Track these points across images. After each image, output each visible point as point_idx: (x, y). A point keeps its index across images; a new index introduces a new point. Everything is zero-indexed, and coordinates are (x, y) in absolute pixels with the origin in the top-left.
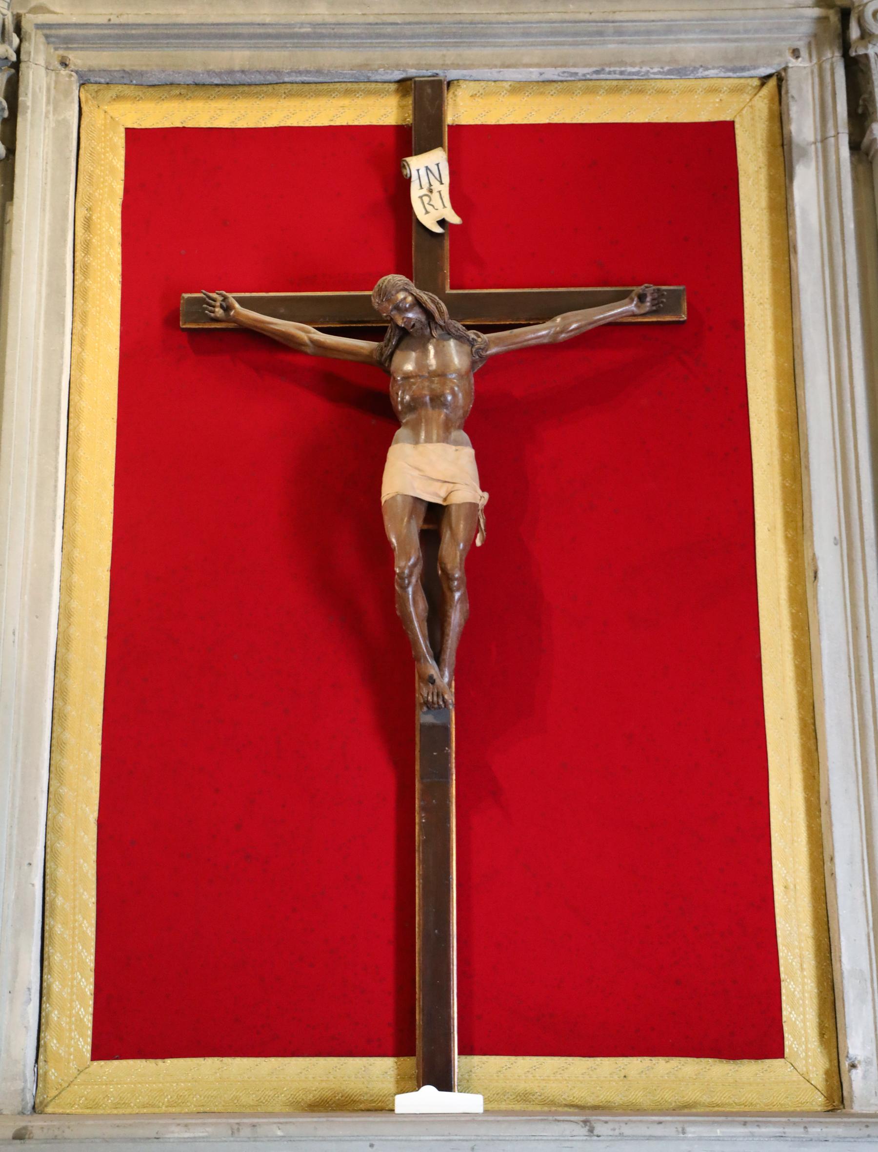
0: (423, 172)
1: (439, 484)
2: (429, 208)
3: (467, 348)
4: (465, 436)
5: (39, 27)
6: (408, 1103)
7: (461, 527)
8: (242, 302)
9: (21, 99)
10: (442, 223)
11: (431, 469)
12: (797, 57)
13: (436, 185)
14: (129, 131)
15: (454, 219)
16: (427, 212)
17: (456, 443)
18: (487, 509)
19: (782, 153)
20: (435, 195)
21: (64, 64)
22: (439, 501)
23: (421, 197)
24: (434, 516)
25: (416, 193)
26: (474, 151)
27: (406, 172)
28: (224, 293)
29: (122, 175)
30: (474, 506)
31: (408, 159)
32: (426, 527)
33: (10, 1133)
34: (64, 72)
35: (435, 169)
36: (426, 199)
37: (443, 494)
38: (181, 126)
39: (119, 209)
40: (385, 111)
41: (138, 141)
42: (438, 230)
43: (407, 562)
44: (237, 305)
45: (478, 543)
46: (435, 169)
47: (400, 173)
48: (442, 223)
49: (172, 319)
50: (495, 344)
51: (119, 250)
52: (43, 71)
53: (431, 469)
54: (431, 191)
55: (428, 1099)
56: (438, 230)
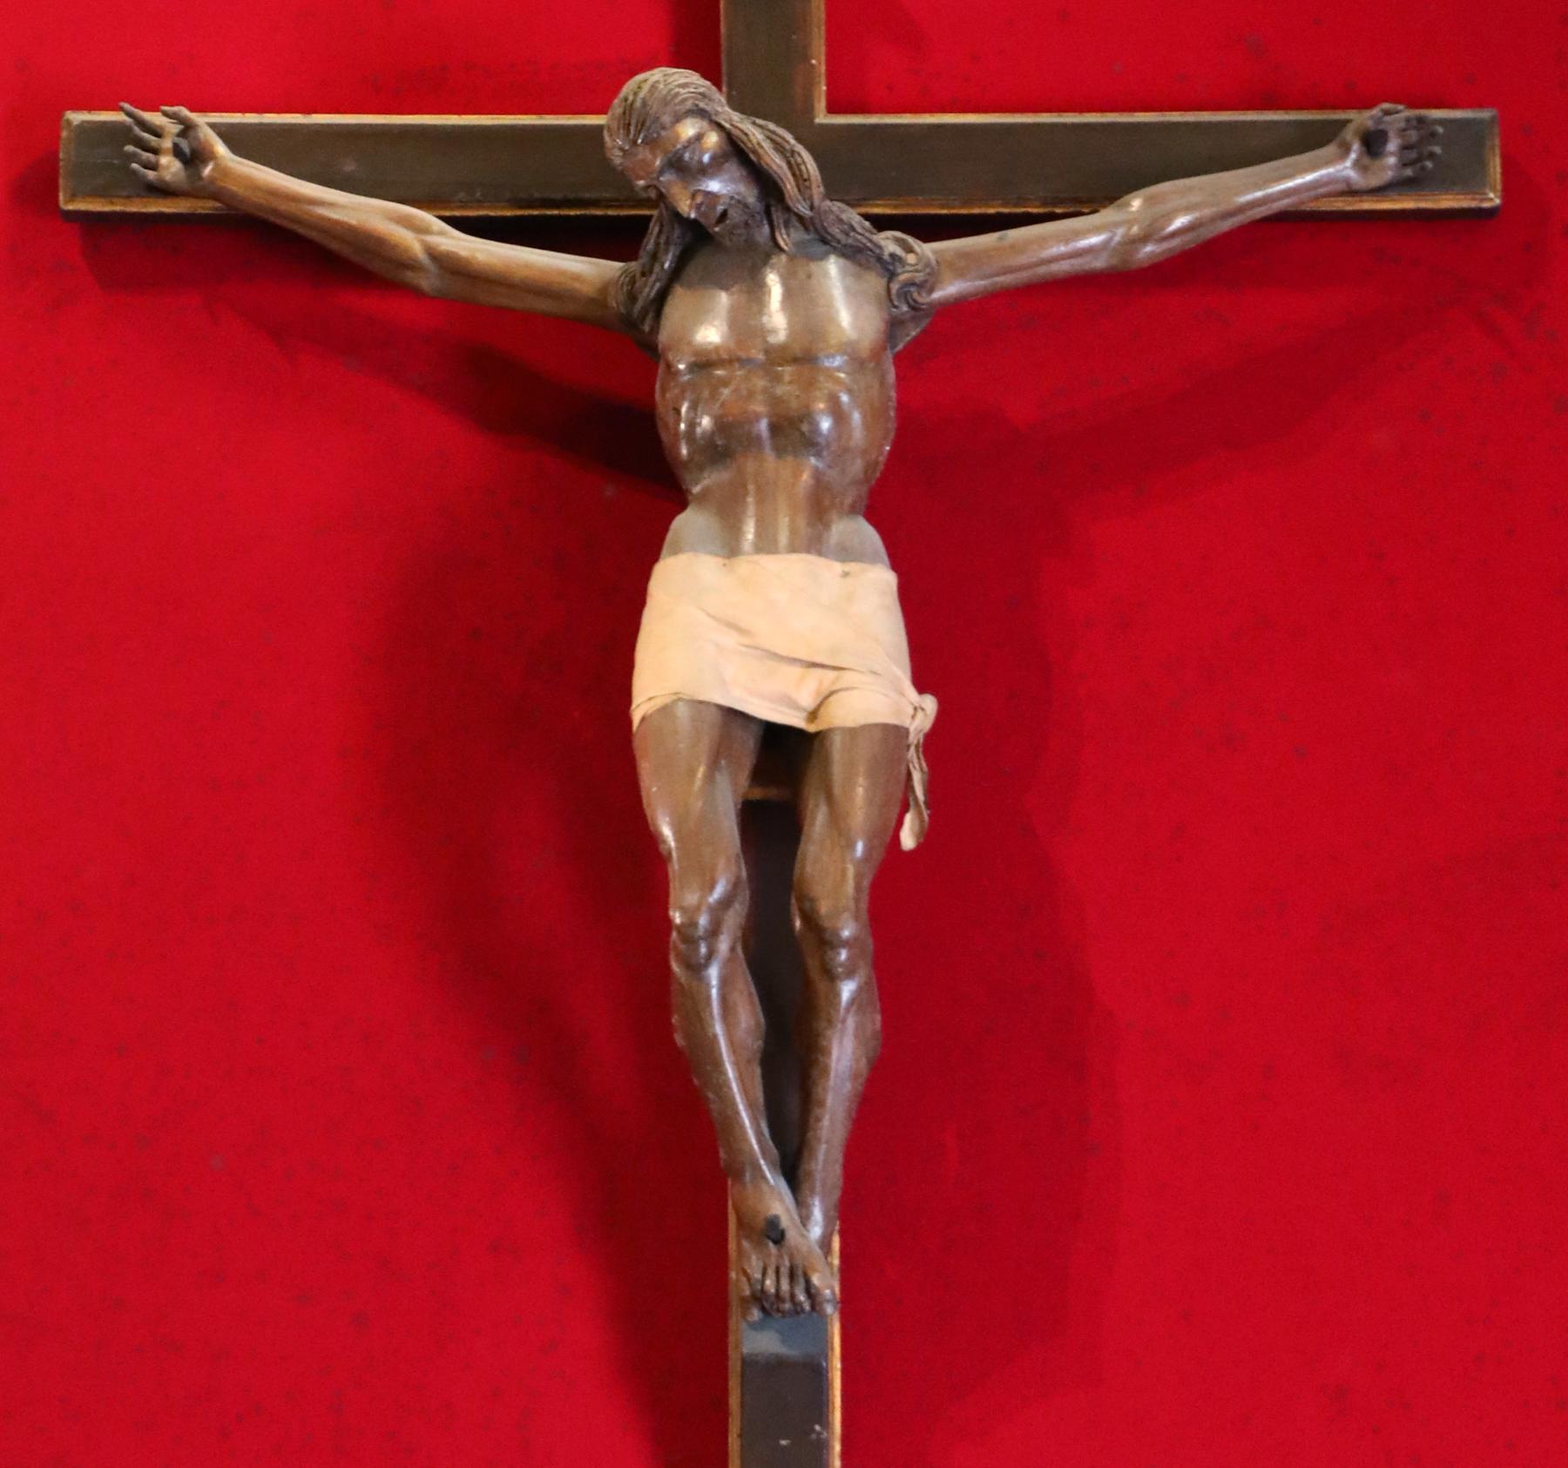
1: (797, 671)
7: (858, 796)
8: (237, 139)
11: (771, 625)
17: (845, 554)
18: (934, 743)
22: (796, 720)
24: (782, 759)
28: (184, 111)
30: (895, 734)
32: (757, 794)
37: (807, 700)
44: (221, 149)
45: (908, 840)
49: (39, 185)
53: (771, 625)
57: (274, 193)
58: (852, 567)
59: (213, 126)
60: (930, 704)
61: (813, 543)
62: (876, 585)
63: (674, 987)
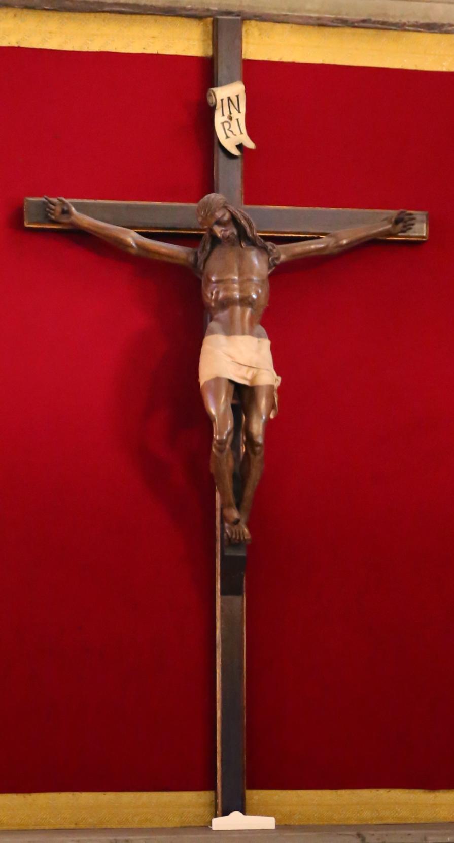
0: (226, 102)
1: (246, 368)
2: (229, 133)
3: (265, 257)
6: (220, 823)
7: (263, 403)
8: (79, 207)
10: (240, 147)
11: (237, 357)
15: (250, 145)
16: (227, 137)
17: (259, 336)
18: (281, 390)
22: (246, 383)
23: (223, 124)
24: (242, 396)
26: (269, 84)
27: (211, 100)
28: (63, 199)
30: (272, 387)
31: (214, 89)
32: (235, 402)
35: (235, 100)
36: (227, 126)
37: (249, 376)
38: (16, 45)
40: (185, 41)
42: (236, 152)
44: (73, 209)
45: (272, 416)
46: (235, 100)
48: (240, 147)
49: (18, 215)
50: (283, 253)
53: (237, 357)
54: (231, 118)
55: (235, 821)
57: (97, 227)
58: (260, 340)
59: (72, 203)
60: (279, 378)
61: (251, 333)
62: (267, 343)
63: (212, 457)
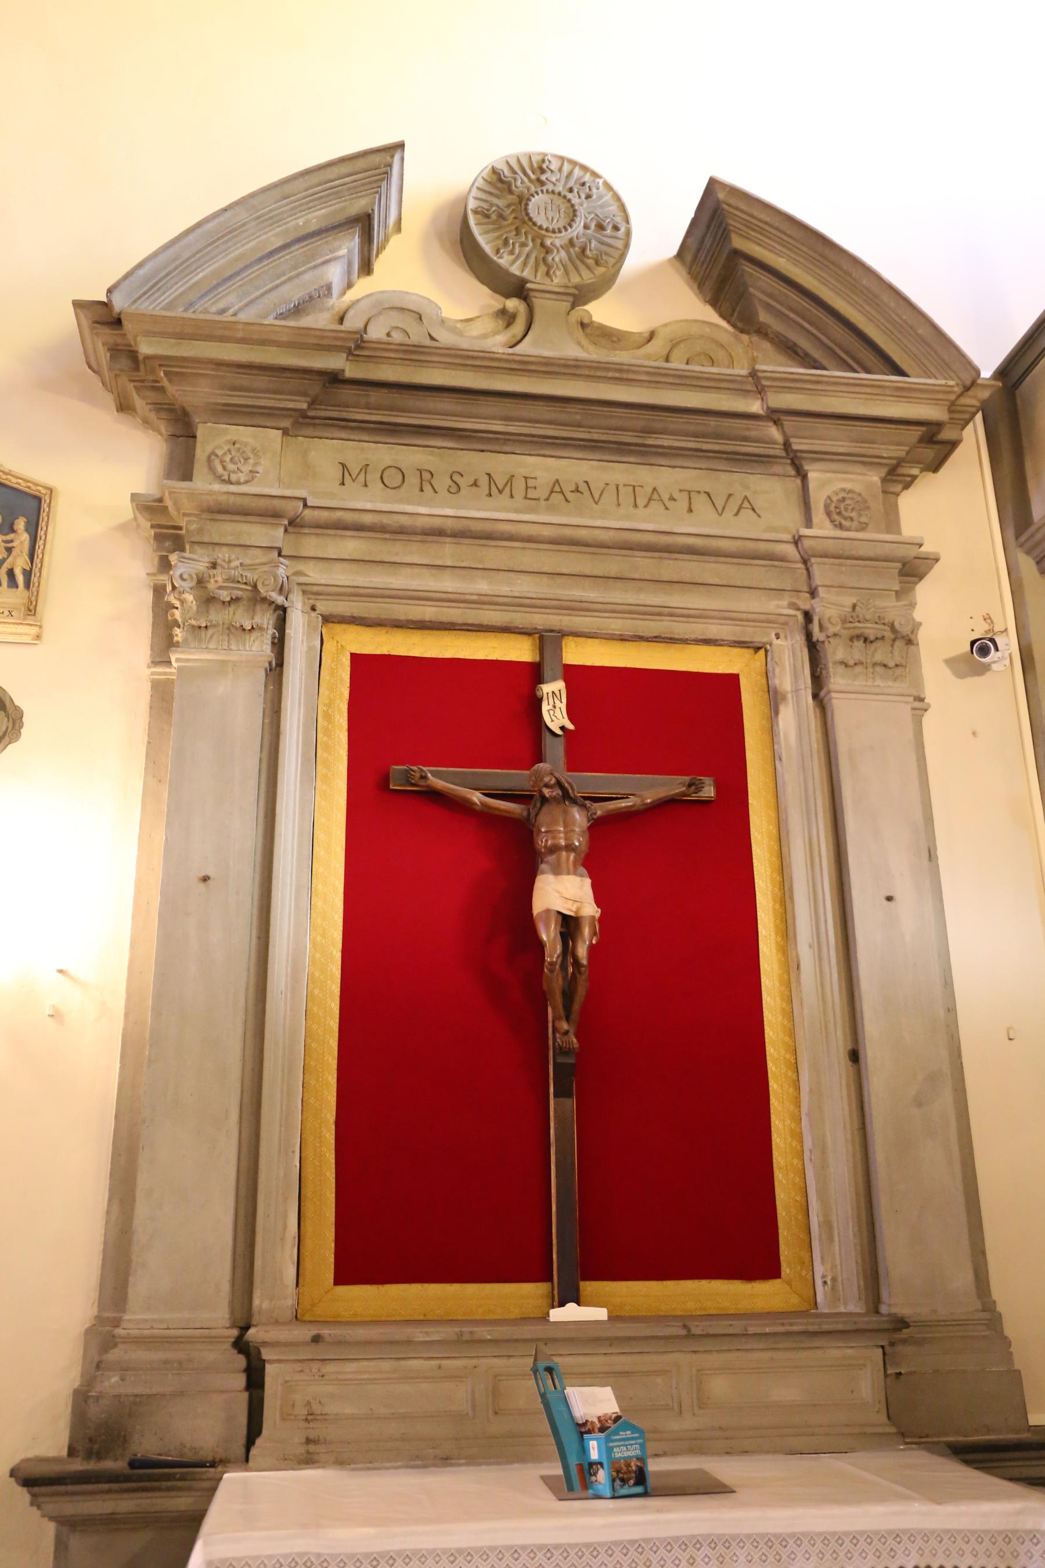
0: (550, 695)
3: (585, 813)
4: (585, 871)
5: (298, 584)
7: (586, 931)
9: (287, 631)
10: (562, 728)
11: (563, 892)
12: (778, 638)
13: (557, 702)
14: (354, 656)
15: (570, 726)
17: (581, 876)
18: (601, 920)
19: (774, 699)
20: (557, 710)
21: (313, 609)
24: (569, 925)
25: (545, 708)
26: (574, 675)
29: (348, 685)
30: (593, 917)
33: (308, 1338)
34: (314, 614)
36: (552, 712)
37: (574, 909)
39: (346, 707)
40: (519, 651)
41: (358, 661)
43: (553, 951)
45: (594, 942)
47: (535, 695)
48: (562, 728)
51: (346, 734)
52: (300, 613)
53: (563, 892)
56: (559, 732)
